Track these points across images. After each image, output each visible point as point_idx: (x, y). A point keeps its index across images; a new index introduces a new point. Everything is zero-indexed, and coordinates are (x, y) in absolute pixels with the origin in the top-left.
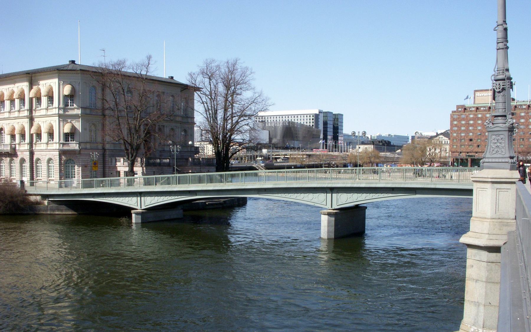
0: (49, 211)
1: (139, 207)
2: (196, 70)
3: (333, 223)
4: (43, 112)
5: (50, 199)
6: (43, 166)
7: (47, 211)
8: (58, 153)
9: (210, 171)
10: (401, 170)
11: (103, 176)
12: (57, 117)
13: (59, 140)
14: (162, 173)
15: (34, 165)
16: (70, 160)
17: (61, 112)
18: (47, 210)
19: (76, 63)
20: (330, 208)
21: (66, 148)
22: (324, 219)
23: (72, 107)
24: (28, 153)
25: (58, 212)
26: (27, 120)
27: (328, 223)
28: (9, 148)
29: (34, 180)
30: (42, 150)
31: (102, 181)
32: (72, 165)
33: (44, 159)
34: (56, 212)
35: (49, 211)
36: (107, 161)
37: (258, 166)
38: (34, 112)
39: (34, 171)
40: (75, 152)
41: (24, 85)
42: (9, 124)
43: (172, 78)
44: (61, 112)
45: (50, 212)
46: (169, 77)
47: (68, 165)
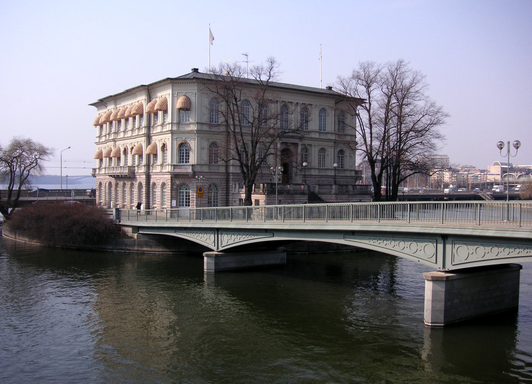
0: (136, 246)
1: (215, 248)
2: (347, 74)
3: (442, 296)
4: (159, 129)
5: (140, 232)
6: (158, 191)
7: (134, 247)
8: (170, 176)
9: (362, 201)
10: (226, 214)
11: (225, 204)
12: (170, 135)
13: (172, 162)
14: (292, 202)
15: (151, 191)
16: (184, 184)
17: (175, 128)
18: (134, 245)
19: (199, 71)
20: (441, 269)
21: (177, 171)
22: (429, 286)
23: (188, 122)
24: (144, 176)
25: (146, 247)
26: (144, 139)
27: (432, 295)
28: (127, 171)
29: (151, 207)
30: (156, 173)
31: (223, 211)
32: (186, 191)
33: (158, 183)
34: (144, 247)
35: (136, 246)
36: (230, 187)
37: (483, 195)
38: (152, 129)
39: (151, 198)
40: (188, 175)
41: (142, 98)
42: (131, 143)
43: (330, 88)
44: (175, 128)
45: (138, 247)
46: (326, 87)
47: (183, 191)
